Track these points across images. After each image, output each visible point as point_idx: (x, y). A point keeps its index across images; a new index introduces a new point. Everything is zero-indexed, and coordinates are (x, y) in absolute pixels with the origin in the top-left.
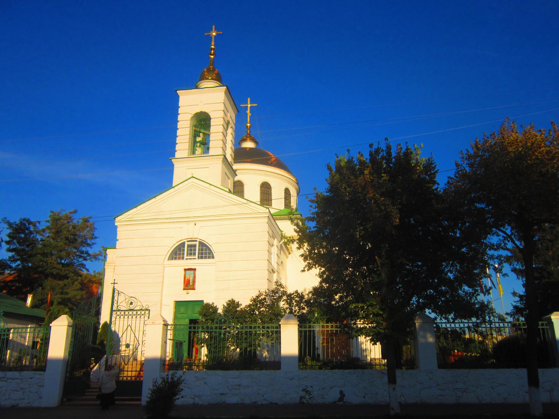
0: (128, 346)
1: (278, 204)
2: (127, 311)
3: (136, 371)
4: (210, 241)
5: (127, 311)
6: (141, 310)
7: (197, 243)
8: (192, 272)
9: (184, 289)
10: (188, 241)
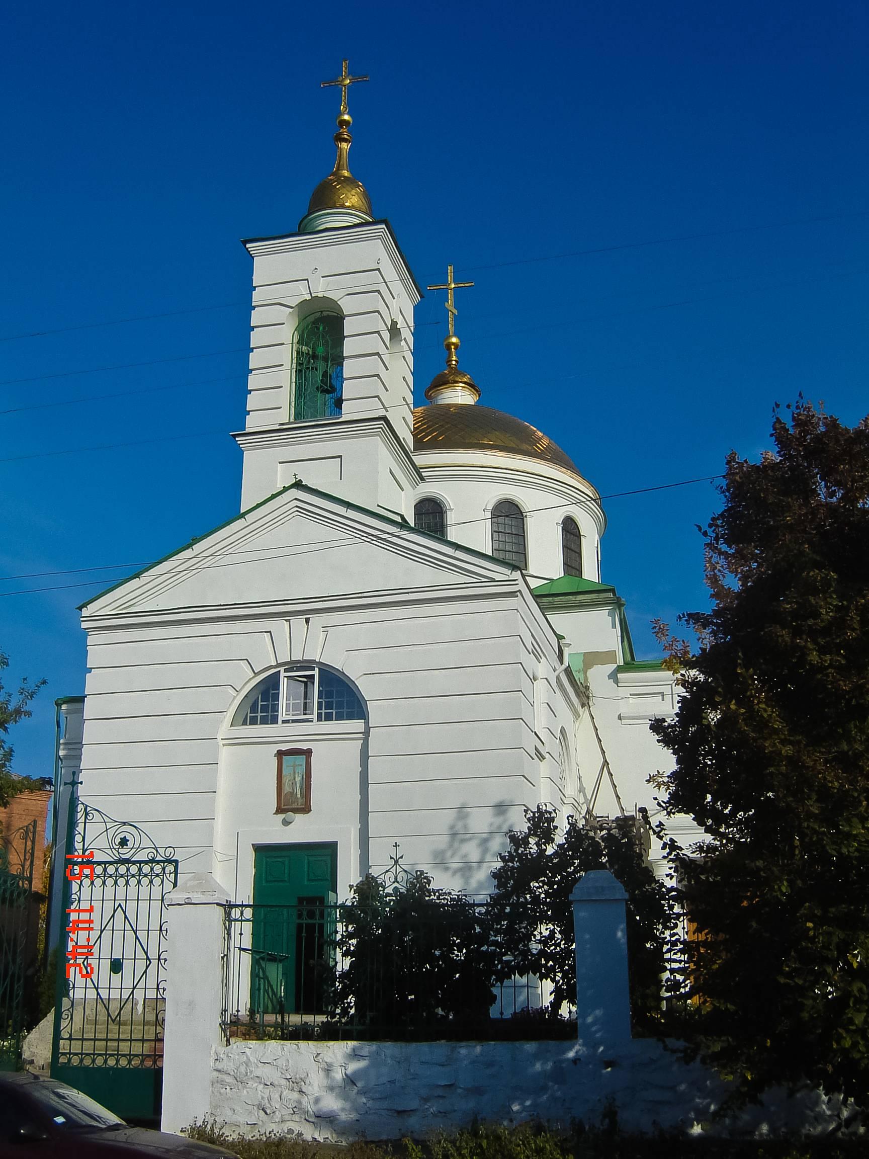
0: (116, 966)
1: (545, 559)
2: (111, 863)
3: (143, 1040)
4: (353, 668)
5: (111, 863)
6: (153, 861)
7: (316, 672)
8: (303, 758)
9: (279, 810)
10: (286, 671)
